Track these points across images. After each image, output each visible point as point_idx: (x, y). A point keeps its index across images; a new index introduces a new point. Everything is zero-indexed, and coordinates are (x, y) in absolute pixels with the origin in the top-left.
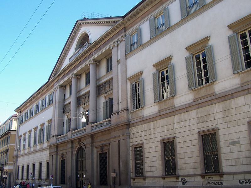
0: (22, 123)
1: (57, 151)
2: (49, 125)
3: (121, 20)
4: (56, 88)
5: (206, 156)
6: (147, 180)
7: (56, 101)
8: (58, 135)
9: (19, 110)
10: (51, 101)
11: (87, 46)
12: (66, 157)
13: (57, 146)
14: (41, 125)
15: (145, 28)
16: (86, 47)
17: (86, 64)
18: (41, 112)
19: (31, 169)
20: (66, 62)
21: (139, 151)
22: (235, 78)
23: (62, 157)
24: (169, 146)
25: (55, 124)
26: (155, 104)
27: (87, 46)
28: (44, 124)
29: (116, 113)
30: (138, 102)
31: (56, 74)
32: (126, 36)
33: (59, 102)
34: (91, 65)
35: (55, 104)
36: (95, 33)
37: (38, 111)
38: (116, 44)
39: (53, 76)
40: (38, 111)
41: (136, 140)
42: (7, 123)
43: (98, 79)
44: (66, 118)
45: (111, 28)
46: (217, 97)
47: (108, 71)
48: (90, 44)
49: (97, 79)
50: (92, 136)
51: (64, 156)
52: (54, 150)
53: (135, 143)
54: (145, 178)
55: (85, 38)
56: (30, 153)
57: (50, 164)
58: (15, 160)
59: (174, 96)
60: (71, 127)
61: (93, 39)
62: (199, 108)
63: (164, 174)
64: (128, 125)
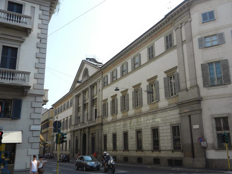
0: (106, 84)
1: (74, 135)
2: (113, 100)
4: (99, 79)
5: (175, 139)
6: (162, 152)
7: (99, 90)
8: (75, 125)
9: (54, 105)
10: (71, 104)
11: (86, 77)
12: (95, 135)
13: (74, 131)
15: (144, 53)
19: (132, 138)
21: (105, 137)
22: (133, 110)
23: (93, 135)
24: (155, 132)
25: (73, 118)
26: (166, 99)
27: (86, 77)
29: (184, 89)
30: (105, 114)
32: (102, 77)
33: (76, 105)
36: (92, 71)
38: (180, 26)
39: (72, 90)
41: (104, 132)
42: (47, 113)
43: (93, 96)
44: (86, 112)
46: (129, 117)
50: (89, 128)
51: (77, 137)
52: (72, 134)
53: (173, 123)
54: (160, 151)
55: (86, 71)
56: (127, 117)
57: (71, 141)
58: (52, 138)
59: (158, 101)
60: (81, 122)
61: (91, 73)
62: (124, 121)
63: (173, 149)
64: (102, 124)
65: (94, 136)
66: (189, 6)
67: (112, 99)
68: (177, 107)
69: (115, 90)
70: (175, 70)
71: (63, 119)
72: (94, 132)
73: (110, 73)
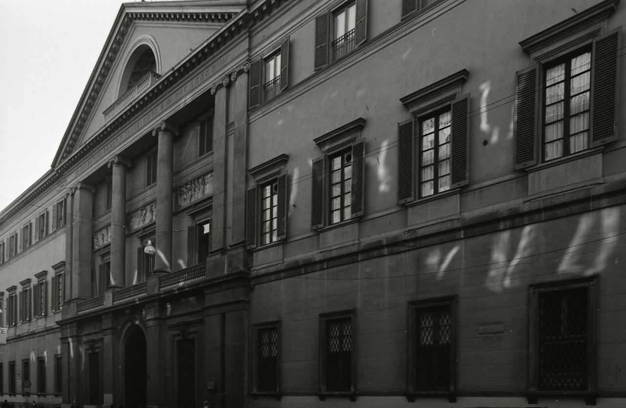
3: (242, 11)
4: (230, 76)
11: (149, 82)
14: (55, 267)
16: (147, 86)
17: (149, 130)
18: (55, 232)
20: (98, 123)
23: (92, 348)
28: (45, 273)
31: (72, 151)
34: (159, 133)
35: (227, 137)
36: (172, 48)
37: (45, 232)
39: (64, 158)
40: (28, 242)
45: (214, 34)
47: (149, 184)
48: (159, 76)
49: (174, 172)
55: (144, 60)
61: (165, 65)
65: (97, 350)
66: (251, 27)
67: (23, 288)
68: (59, 329)
69: (572, 9)
70: (28, 285)
71: (22, 283)
72: (95, 337)
73: (52, 206)
